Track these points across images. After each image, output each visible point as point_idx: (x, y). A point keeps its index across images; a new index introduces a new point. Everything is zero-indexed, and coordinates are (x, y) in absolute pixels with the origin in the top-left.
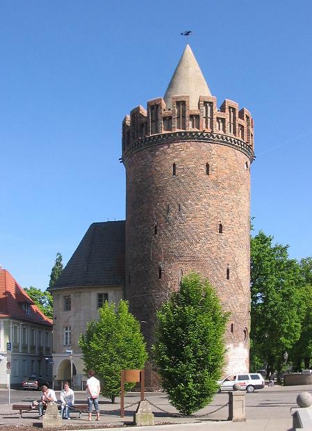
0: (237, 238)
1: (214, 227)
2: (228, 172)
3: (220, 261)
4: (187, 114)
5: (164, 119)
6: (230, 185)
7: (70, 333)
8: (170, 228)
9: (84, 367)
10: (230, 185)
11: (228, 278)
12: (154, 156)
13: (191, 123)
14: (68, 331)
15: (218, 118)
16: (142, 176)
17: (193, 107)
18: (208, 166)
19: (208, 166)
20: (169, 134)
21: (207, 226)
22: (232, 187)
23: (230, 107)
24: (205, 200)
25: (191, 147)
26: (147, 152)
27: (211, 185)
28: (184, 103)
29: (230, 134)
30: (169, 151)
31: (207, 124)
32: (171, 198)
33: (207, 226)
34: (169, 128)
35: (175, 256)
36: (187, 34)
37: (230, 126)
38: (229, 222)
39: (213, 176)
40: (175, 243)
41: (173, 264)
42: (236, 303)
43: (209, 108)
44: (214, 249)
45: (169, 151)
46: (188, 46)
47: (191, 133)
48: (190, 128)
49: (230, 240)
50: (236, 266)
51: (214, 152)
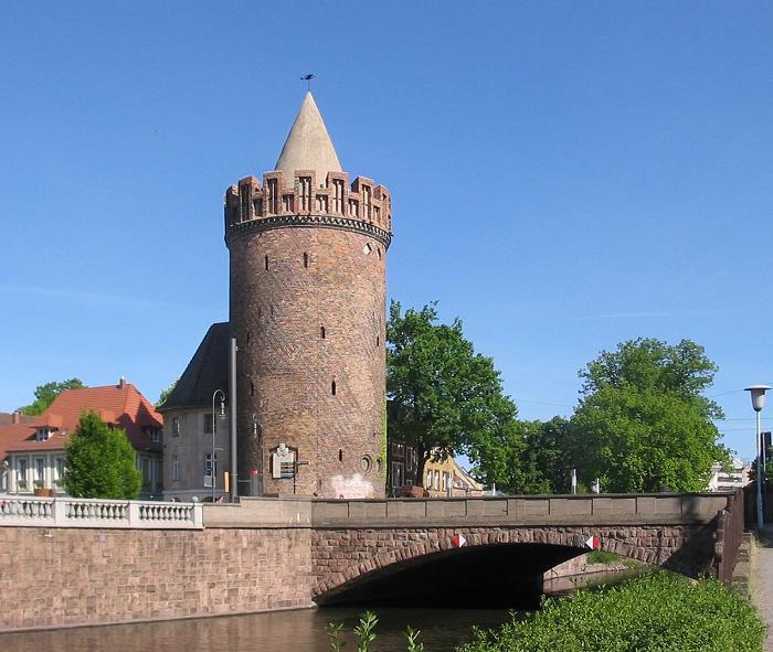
1: (312, 329)
2: (333, 261)
5: (255, 202)
6: (336, 277)
10: (336, 277)
11: (334, 393)
12: (246, 246)
13: (284, 205)
15: (350, 200)
17: (319, 181)
18: (305, 255)
19: (305, 255)
20: (260, 221)
22: (340, 280)
23: (363, 186)
25: (285, 235)
27: (310, 280)
28: (309, 179)
29: (335, 211)
30: (261, 240)
31: (304, 204)
34: (260, 213)
35: (267, 369)
36: (309, 77)
37: (304, 200)
39: (312, 268)
40: (268, 353)
41: (265, 379)
43: (307, 184)
44: (313, 359)
45: (261, 240)
46: (310, 94)
47: (283, 218)
48: (284, 211)
50: (345, 379)
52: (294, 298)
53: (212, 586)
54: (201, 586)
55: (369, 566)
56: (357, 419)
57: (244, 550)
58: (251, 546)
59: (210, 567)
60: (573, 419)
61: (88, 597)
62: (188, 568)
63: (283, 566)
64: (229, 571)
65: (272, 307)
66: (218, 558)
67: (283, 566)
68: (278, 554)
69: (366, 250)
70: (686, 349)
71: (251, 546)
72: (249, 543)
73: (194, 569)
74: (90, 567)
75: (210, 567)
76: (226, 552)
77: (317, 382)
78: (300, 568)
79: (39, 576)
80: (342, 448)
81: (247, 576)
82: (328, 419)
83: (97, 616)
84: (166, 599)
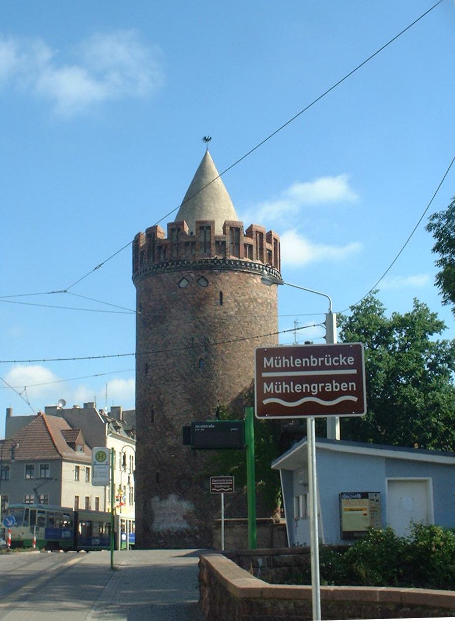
11: (153, 421)
49: (155, 378)
80: (159, 471)
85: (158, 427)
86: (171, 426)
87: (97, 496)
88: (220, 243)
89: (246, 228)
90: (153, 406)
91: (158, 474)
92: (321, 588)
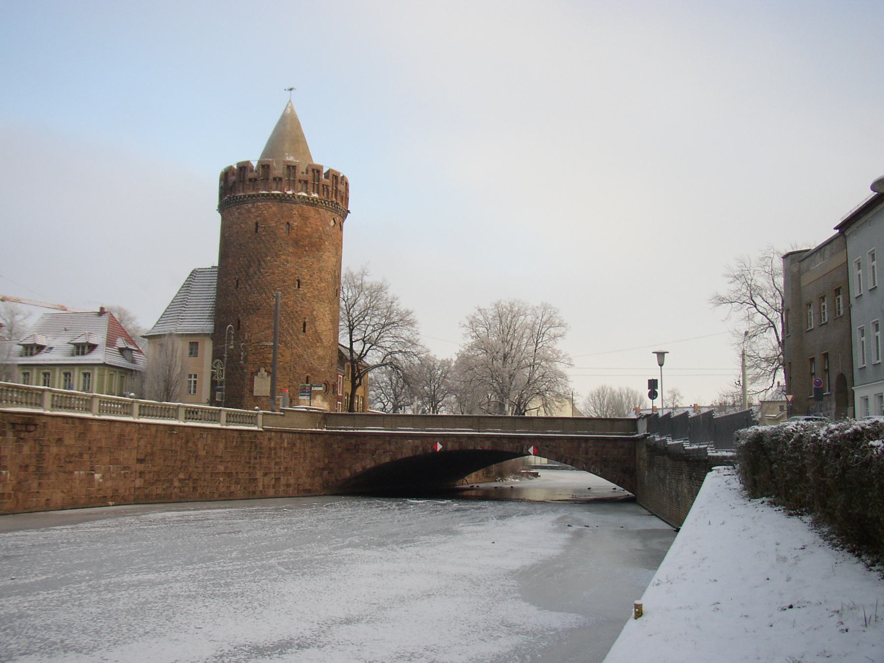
0: (316, 293)
3: (297, 315)
4: (271, 177)
7: (195, 382)
8: (250, 282)
9: (536, 608)
11: (304, 331)
14: (193, 379)
16: (229, 231)
21: (284, 282)
24: (283, 257)
26: (234, 210)
32: (252, 254)
33: (284, 282)
36: (291, 89)
38: (308, 277)
42: (312, 356)
49: (308, 295)
51: (295, 212)
52: (277, 256)
53: (265, 474)
54: (259, 475)
55: (369, 464)
56: (321, 352)
57: (285, 449)
58: (289, 446)
59: (264, 460)
60: (465, 362)
61: (194, 479)
62: (252, 461)
63: (307, 462)
64: (276, 464)
65: (259, 261)
66: (270, 454)
67: (307, 462)
68: (305, 453)
69: (332, 223)
70: (545, 309)
71: (289, 446)
72: (288, 443)
73: (256, 461)
74: (196, 457)
75: (264, 460)
76: (275, 449)
77: (292, 322)
78: (317, 464)
79: (166, 462)
80: (309, 375)
81: (286, 468)
82: (300, 350)
83: (198, 494)
84: (239, 484)
85: (310, 338)
86: (321, 339)
87: (193, 359)
88: (277, 179)
89: (325, 171)
90: (305, 318)
91: (308, 377)
92: (49, 406)
